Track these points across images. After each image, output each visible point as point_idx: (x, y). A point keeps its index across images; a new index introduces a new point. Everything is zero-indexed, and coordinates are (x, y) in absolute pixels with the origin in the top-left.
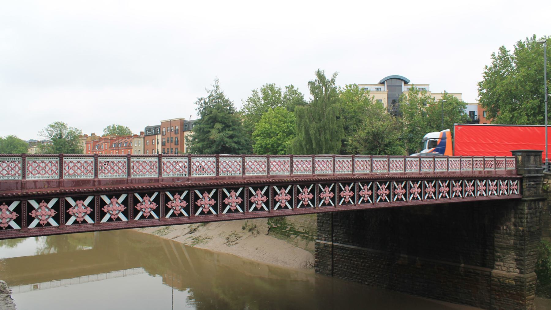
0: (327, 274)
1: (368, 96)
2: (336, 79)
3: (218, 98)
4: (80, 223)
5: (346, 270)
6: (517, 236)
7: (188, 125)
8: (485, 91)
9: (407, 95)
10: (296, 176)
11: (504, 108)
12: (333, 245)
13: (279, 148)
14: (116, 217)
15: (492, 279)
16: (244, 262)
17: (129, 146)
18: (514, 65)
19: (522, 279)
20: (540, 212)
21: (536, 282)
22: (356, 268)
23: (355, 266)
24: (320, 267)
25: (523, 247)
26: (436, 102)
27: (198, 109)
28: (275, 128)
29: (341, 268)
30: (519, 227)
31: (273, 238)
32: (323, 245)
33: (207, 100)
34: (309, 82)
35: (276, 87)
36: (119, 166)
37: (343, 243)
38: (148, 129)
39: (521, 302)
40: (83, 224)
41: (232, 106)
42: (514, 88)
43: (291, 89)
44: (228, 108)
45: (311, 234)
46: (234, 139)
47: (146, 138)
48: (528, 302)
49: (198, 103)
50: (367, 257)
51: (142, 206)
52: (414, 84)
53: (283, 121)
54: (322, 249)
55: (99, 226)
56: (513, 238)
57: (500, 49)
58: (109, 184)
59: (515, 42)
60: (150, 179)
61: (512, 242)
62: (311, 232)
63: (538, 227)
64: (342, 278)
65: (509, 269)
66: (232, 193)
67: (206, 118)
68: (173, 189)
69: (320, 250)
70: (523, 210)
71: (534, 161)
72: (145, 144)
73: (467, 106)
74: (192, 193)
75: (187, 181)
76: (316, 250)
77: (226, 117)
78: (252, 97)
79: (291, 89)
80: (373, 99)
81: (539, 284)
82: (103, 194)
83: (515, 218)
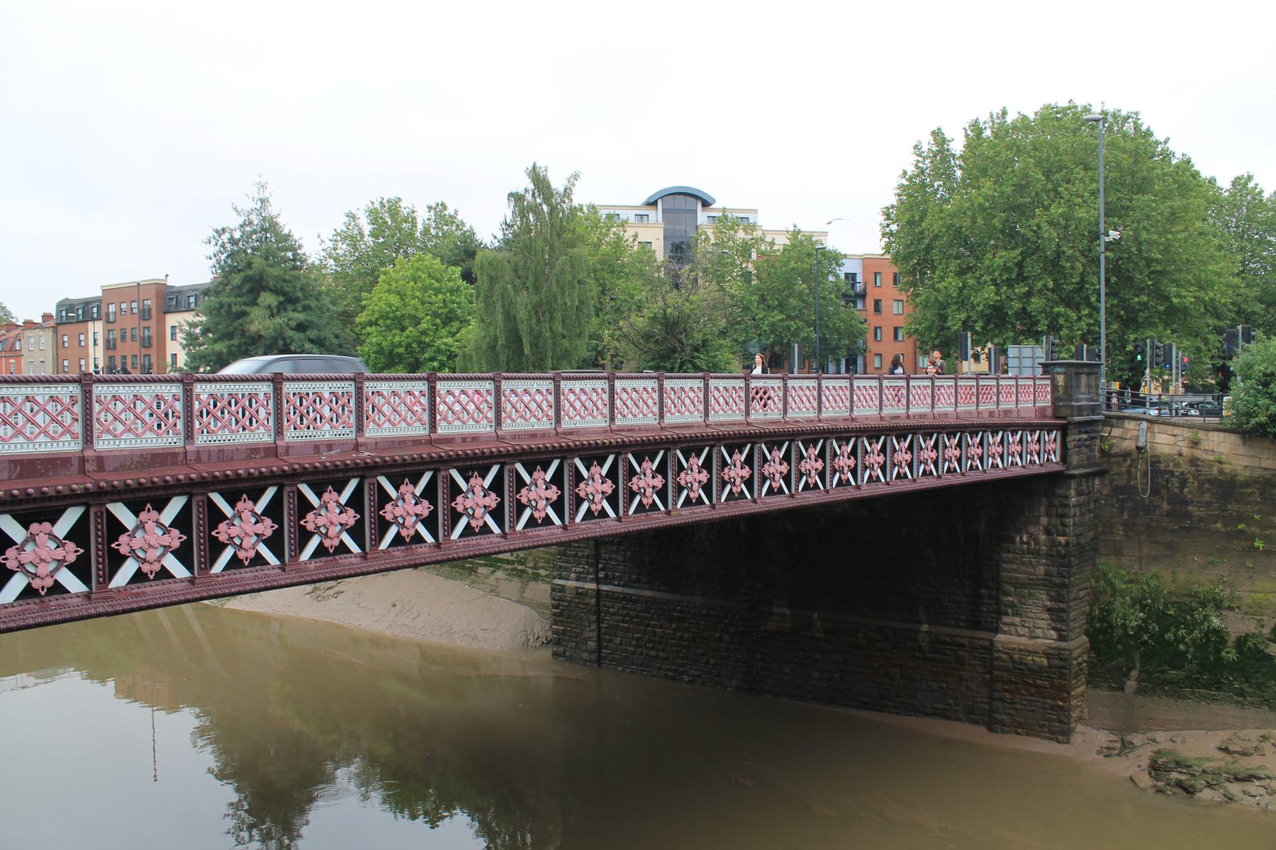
0: (586, 661)
1: (622, 233)
2: (575, 190)
3: (264, 230)
4: (43, 593)
5: (633, 649)
6: (1052, 556)
7: (177, 297)
8: (894, 227)
9: (710, 232)
10: (623, 430)
11: (944, 266)
12: (598, 591)
13: (426, 356)
14: (157, 567)
15: (996, 655)
16: (355, 639)
17: (11, 350)
18: (959, 173)
19: (1062, 652)
20: (1096, 501)
21: (1089, 657)
22: (660, 645)
23: (657, 639)
24: (566, 646)
25: (1066, 580)
26: (779, 250)
27: (215, 255)
28: (414, 305)
29: (621, 643)
30: (1058, 535)
31: (431, 576)
32: (573, 592)
33: (237, 235)
34: (511, 195)
35: (404, 209)
36: (139, 410)
37: (623, 586)
38: (67, 306)
39: (1061, 703)
40: (52, 598)
41: (298, 251)
42: (967, 223)
43: (441, 211)
44: (290, 255)
45: (531, 564)
46: (308, 333)
47: (61, 328)
48: (1074, 703)
49: (213, 242)
50: (688, 616)
51: (234, 531)
52: (727, 207)
53: (435, 289)
54: (570, 601)
55: (106, 598)
56: (1044, 561)
57: (933, 133)
58: (130, 468)
59: (966, 122)
60: (252, 449)
61: (1041, 570)
62: (530, 558)
63: (1091, 534)
64: (624, 670)
65: (1034, 631)
66: (473, 481)
67: (237, 279)
68: (321, 477)
69: (566, 604)
70: (1066, 497)
71: (1086, 386)
72: (58, 345)
73: (843, 261)
74: (371, 484)
75: (353, 449)
76: (556, 603)
77: (287, 277)
78: (345, 229)
79: (439, 210)
80: (634, 240)
81: (1094, 660)
82: (116, 497)
83: (1048, 515)
